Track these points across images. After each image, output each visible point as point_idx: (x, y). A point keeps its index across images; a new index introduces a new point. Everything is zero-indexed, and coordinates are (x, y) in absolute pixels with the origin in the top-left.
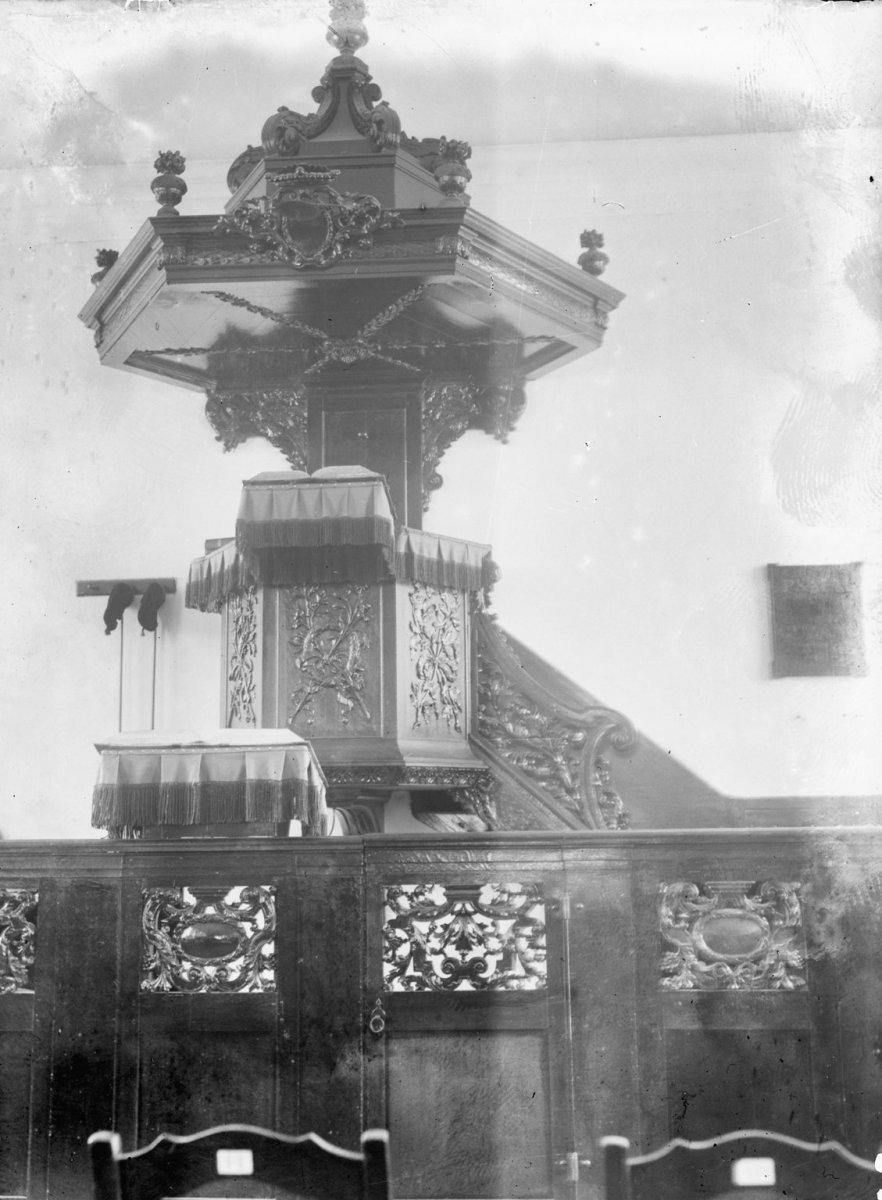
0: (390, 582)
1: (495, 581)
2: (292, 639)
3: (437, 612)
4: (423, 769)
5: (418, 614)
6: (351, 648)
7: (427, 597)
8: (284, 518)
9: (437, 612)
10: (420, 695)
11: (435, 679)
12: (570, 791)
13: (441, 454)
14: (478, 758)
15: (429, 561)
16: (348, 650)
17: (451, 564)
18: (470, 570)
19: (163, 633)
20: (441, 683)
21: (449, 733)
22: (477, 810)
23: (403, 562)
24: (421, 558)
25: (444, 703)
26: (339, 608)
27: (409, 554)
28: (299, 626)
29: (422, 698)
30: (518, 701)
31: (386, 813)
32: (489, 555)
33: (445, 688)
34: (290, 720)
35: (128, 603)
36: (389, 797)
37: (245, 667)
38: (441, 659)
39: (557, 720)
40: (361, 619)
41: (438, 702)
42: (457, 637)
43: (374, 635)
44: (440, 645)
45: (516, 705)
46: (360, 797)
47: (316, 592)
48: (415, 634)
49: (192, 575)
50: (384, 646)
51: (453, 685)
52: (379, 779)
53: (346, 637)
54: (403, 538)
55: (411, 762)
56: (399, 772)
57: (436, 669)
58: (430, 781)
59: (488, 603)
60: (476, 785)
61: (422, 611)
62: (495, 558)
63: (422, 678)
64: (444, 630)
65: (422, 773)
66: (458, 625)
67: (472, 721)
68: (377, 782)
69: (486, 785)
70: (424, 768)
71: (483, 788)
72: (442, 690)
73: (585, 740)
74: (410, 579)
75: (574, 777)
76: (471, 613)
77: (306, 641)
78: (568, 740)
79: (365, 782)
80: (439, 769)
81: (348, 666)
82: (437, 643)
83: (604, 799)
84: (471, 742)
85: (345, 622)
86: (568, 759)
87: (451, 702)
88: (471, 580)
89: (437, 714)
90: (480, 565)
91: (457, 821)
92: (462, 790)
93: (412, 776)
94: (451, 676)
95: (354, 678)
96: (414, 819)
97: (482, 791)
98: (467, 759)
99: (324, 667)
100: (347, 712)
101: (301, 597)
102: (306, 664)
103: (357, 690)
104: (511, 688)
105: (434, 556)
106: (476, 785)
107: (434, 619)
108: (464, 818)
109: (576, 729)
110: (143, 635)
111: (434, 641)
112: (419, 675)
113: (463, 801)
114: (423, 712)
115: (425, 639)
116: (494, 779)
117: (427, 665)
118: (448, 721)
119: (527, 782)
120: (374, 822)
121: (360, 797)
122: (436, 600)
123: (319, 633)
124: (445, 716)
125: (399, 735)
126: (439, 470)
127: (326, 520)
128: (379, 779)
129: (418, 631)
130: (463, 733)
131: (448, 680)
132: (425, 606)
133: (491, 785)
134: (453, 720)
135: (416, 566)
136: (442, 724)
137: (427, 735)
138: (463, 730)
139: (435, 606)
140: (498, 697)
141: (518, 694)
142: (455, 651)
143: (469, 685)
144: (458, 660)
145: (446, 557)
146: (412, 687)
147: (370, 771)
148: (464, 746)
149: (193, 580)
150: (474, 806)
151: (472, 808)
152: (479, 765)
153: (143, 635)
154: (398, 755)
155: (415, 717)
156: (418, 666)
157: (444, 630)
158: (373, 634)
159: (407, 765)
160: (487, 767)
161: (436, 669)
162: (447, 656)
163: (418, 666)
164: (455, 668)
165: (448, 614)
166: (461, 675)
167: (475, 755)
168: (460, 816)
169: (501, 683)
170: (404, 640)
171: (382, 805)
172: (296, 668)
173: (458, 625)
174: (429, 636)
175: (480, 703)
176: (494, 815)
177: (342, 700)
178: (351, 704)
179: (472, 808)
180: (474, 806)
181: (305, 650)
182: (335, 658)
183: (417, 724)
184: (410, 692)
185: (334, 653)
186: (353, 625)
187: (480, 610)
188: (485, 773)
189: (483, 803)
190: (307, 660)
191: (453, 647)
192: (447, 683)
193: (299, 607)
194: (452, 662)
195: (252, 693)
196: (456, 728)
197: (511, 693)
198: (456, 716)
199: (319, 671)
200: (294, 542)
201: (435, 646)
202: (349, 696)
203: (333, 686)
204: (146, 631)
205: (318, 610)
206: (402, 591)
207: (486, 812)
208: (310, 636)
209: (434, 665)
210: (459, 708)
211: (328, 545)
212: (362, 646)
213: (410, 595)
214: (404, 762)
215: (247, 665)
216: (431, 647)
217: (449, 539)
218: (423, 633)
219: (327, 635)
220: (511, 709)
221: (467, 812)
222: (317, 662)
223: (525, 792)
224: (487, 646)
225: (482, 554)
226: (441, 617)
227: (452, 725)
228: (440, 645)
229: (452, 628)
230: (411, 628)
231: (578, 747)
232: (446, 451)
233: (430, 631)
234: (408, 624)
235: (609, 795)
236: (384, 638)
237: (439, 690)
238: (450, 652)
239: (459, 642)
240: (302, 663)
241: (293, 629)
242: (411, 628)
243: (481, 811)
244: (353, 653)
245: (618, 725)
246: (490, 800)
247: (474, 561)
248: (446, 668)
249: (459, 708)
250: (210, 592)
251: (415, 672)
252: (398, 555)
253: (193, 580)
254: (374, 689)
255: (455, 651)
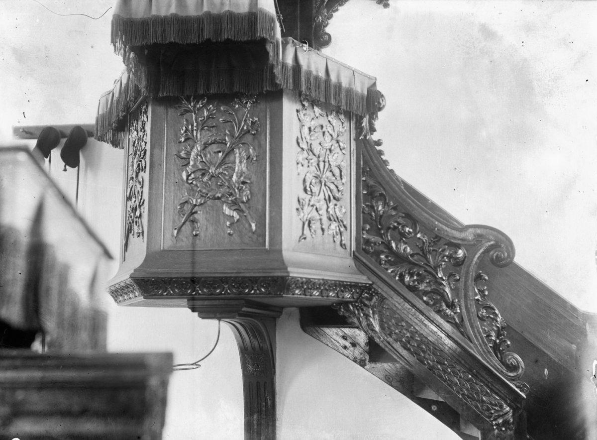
0: (276, 95)
1: (380, 109)
2: (179, 152)
3: (324, 133)
4: (309, 281)
5: (306, 130)
6: (237, 161)
7: (314, 117)
8: (163, 13)
9: (324, 133)
10: (307, 209)
11: (322, 196)
12: (451, 306)
13: (330, 17)
14: (362, 273)
15: (317, 78)
16: (234, 162)
17: (339, 86)
18: (356, 95)
19: (86, 170)
20: (328, 200)
21: (335, 249)
22: (360, 323)
23: (290, 73)
24: (309, 73)
25: (330, 219)
26: (226, 122)
27: (297, 67)
28: (186, 140)
29: (308, 213)
30: (400, 220)
31: (277, 328)
32: (374, 84)
33: (331, 205)
34: (175, 232)
35: (54, 145)
36: (281, 312)
37: (137, 184)
38: (327, 178)
39: (437, 238)
40: (248, 132)
41: (325, 218)
42: (343, 159)
43: (261, 147)
44: (327, 164)
45: (399, 224)
46: (244, 309)
47: (204, 106)
48: (303, 149)
49: (100, 110)
50: (271, 158)
51: (338, 203)
52: (263, 290)
53: (232, 150)
54: (290, 51)
55: (295, 273)
56: (282, 283)
57: (323, 186)
58: (316, 293)
59: (372, 130)
60: (360, 300)
61: (310, 129)
62: (379, 88)
63: (309, 193)
64: (330, 150)
65: (307, 285)
66: (344, 148)
67: (357, 240)
68: (262, 293)
69: (370, 299)
70: (309, 279)
71: (366, 302)
72: (328, 207)
73: (465, 257)
74: (299, 96)
75: (455, 291)
76: (356, 139)
77: (193, 154)
78: (450, 257)
79: (249, 293)
80: (325, 282)
81: (234, 178)
82: (324, 162)
83: (484, 312)
84: (356, 258)
85: (232, 136)
86: (450, 276)
87: (337, 220)
88: (359, 108)
89: (323, 230)
90: (366, 93)
91: (341, 334)
92: (346, 304)
93: (297, 288)
94: (337, 195)
95: (240, 190)
96: (301, 330)
97: (365, 305)
98: (352, 274)
99: (210, 179)
100: (232, 224)
101: (188, 111)
102: (193, 176)
103: (243, 202)
104: (395, 208)
105: (322, 74)
106: (360, 300)
107: (321, 139)
108: (347, 331)
109: (458, 246)
110: (65, 170)
111: (321, 159)
112: (305, 190)
113: (347, 314)
114: (309, 226)
115: (311, 156)
116: (377, 294)
117: (314, 181)
118: (334, 237)
119: (410, 296)
120: (265, 334)
121: (244, 309)
122: (323, 121)
123: (206, 146)
124: (331, 232)
125: (285, 246)
126: (328, 30)
127: (208, 14)
128: (263, 290)
129: (304, 146)
130: (348, 248)
131: (334, 198)
132: (313, 124)
133: (374, 299)
134: (338, 237)
135: (303, 79)
136: (328, 238)
137: (313, 250)
138: (348, 248)
139: (322, 127)
140: (381, 216)
141: (401, 214)
142: (341, 171)
143: (354, 205)
144: (344, 181)
145: (333, 78)
146: (299, 201)
147: (254, 281)
148: (349, 262)
149: (100, 113)
150: (358, 319)
151: (355, 320)
152: (363, 279)
153: (65, 170)
154: (283, 266)
155: (301, 231)
156: (304, 181)
157: (330, 150)
158: (260, 145)
159: (291, 275)
160: (370, 282)
161: (323, 186)
162: (334, 175)
163: (304, 181)
164: (341, 188)
165: (335, 136)
166: (347, 195)
167: (358, 269)
168: (343, 329)
169: (385, 204)
170: (290, 153)
171: (274, 319)
172: (182, 180)
173: (344, 148)
174: (317, 153)
175: (364, 223)
176: (377, 328)
177: (227, 211)
178: (236, 215)
179: (355, 320)
180: (358, 319)
181: (192, 163)
182: (221, 170)
183: (303, 237)
184: (296, 205)
185: (220, 165)
186: (240, 137)
187: (365, 136)
188: (368, 288)
189: (367, 316)
190: (194, 172)
191: (339, 169)
192: (333, 201)
193: (187, 120)
194: (338, 183)
195: (142, 208)
196: (341, 245)
197: (394, 213)
198: (341, 233)
199: (206, 183)
200: (172, 38)
201: (322, 164)
202: (233, 208)
203: (219, 198)
204: (67, 167)
205: (202, 126)
206: (289, 107)
207: (370, 325)
208: (198, 147)
209: (321, 182)
210: (345, 227)
211: (209, 40)
212: (248, 158)
213: (298, 111)
214: (288, 272)
215: (140, 182)
216: (318, 165)
217: (337, 62)
218: (311, 150)
219: (215, 148)
220: (395, 228)
221: (351, 326)
222: (203, 175)
223: (407, 306)
224: (375, 182)
225: (367, 84)
226: (328, 138)
227: (338, 242)
228: (327, 164)
229: (338, 150)
230: (298, 144)
231: (459, 263)
232: (335, 14)
233: (317, 149)
234: (296, 138)
235: (488, 308)
236: (271, 150)
237: (325, 207)
238: (337, 172)
239: (345, 165)
240: (188, 176)
241: (180, 142)
242: (298, 144)
243: (364, 323)
244: (240, 167)
245: (497, 242)
246: (373, 314)
247: (360, 88)
248: (333, 187)
249: (345, 227)
250: (119, 122)
251: (302, 187)
252: (284, 65)
253: (100, 113)
254: (260, 199)
255: (341, 171)
